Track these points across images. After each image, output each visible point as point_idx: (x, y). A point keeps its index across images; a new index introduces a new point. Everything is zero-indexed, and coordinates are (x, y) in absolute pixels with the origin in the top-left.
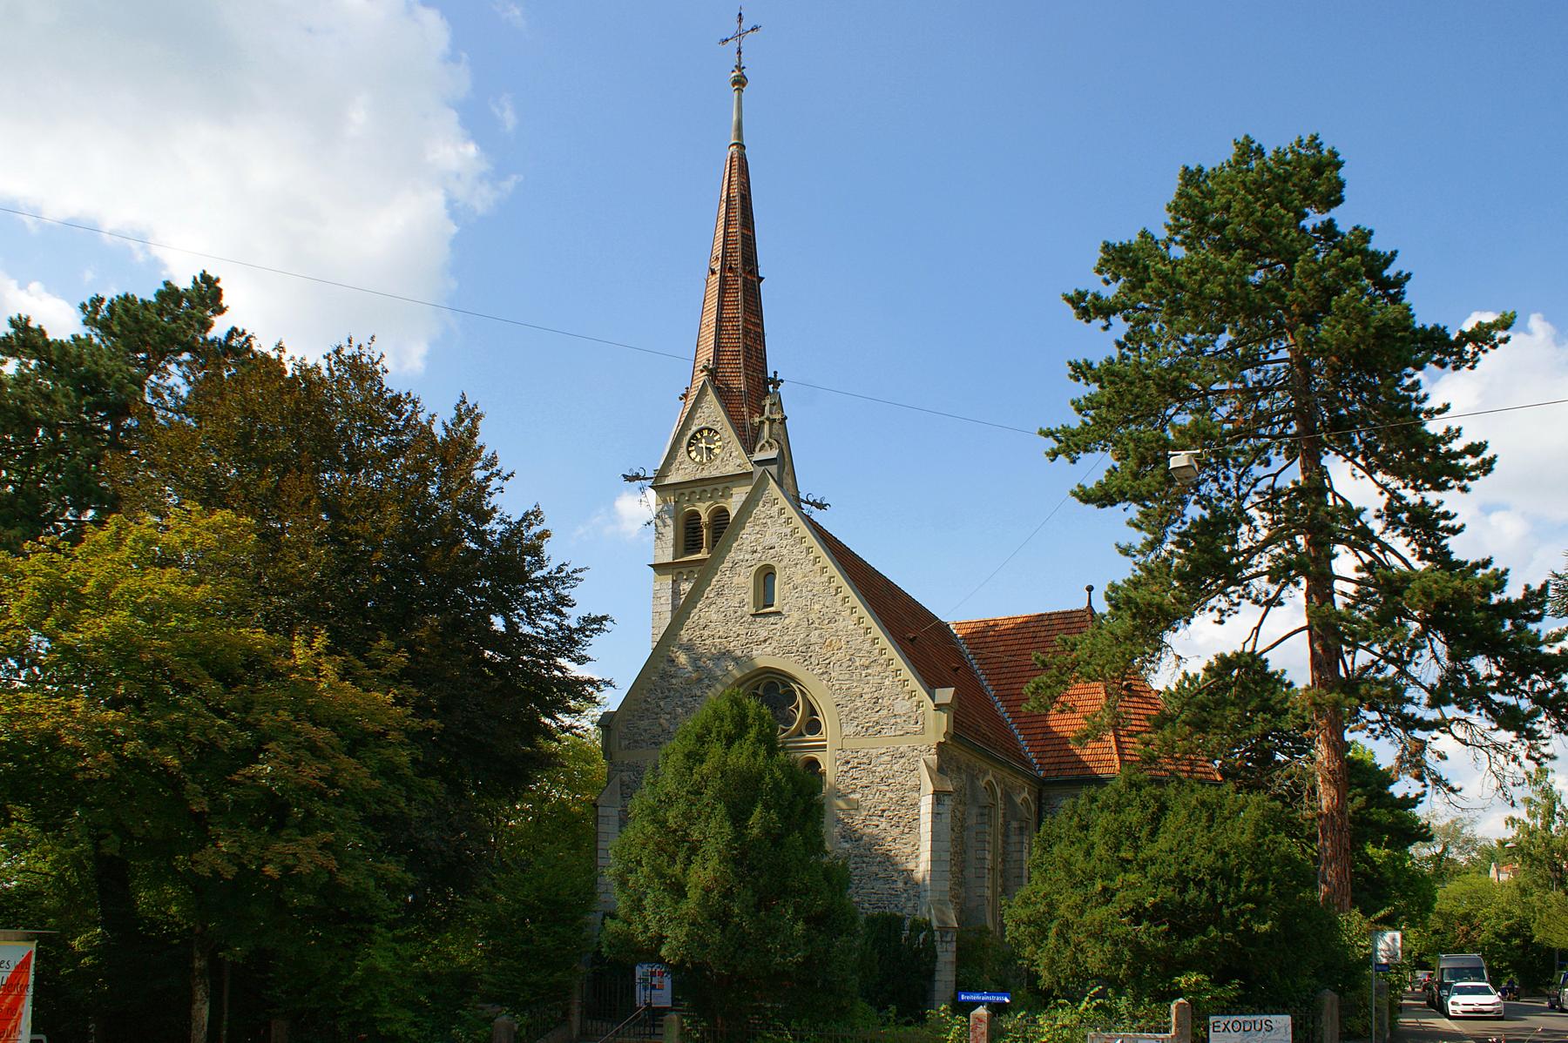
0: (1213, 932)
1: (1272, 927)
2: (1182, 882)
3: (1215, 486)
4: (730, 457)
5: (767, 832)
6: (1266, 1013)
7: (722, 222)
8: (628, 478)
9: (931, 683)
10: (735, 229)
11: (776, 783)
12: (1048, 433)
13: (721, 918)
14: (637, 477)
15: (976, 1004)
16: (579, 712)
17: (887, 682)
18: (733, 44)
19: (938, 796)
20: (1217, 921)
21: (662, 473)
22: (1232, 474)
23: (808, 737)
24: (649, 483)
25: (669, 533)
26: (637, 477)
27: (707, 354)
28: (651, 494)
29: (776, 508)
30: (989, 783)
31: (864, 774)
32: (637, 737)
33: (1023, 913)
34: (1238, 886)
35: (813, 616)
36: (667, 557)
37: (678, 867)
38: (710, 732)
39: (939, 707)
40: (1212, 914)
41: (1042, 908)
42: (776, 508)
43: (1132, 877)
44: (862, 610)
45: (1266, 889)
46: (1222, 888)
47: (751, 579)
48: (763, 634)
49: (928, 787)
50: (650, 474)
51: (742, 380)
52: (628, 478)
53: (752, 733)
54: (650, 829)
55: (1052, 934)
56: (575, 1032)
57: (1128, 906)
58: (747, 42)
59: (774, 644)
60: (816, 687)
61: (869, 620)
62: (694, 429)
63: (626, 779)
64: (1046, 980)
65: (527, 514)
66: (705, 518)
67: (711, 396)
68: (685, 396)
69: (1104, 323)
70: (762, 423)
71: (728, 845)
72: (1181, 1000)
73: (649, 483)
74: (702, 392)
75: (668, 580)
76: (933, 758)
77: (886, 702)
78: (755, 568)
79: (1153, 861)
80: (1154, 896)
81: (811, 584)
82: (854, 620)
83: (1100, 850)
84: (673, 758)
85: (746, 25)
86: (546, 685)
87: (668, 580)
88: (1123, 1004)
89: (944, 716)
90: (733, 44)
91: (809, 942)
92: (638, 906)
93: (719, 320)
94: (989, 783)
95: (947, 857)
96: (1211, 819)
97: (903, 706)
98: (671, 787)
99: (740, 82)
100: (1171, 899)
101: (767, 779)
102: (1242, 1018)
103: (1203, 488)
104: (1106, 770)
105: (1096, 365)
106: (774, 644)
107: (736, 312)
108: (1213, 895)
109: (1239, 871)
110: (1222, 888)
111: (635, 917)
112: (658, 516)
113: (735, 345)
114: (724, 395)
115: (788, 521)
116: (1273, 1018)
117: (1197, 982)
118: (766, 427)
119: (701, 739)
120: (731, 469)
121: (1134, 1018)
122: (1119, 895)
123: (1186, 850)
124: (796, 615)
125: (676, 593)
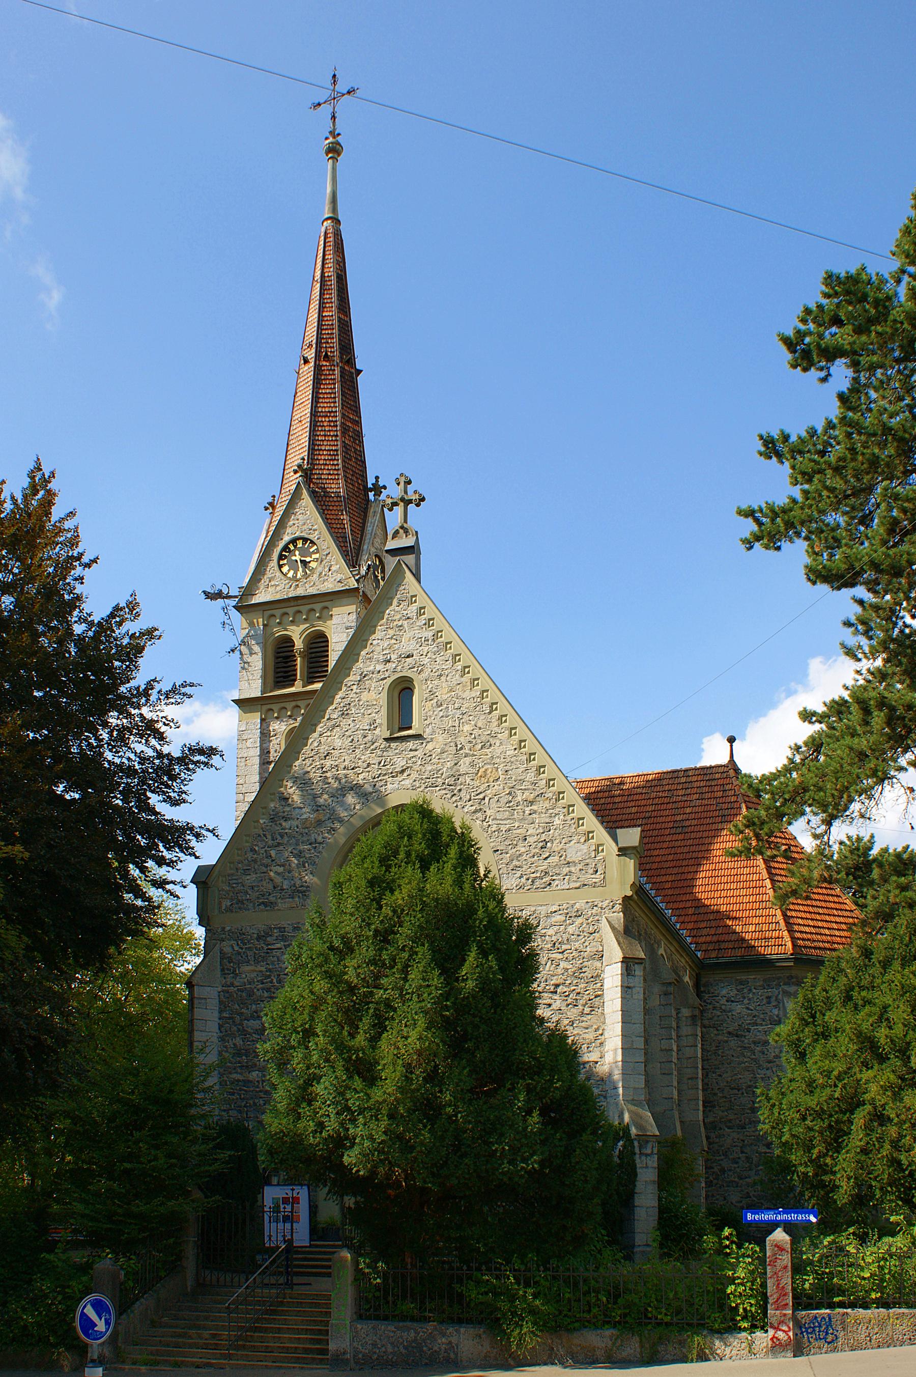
4: (330, 572)
5: (484, 984)
7: (315, 305)
8: (208, 595)
10: (332, 313)
12: (750, 513)
13: (428, 1109)
14: (219, 595)
15: (772, 1226)
16: (171, 864)
17: (557, 821)
18: (326, 109)
19: (628, 963)
21: (249, 590)
24: (233, 602)
25: (257, 662)
26: (219, 595)
27: (299, 453)
28: (235, 615)
29: (414, 607)
32: (241, 897)
35: (462, 740)
36: (254, 690)
37: (360, 1040)
38: (396, 853)
39: (623, 852)
42: (414, 607)
48: (400, 763)
49: (614, 952)
50: (234, 592)
51: (342, 486)
52: (209, 596)
54: (321, 985)
56: (190, 1283)
59: (414, 775)
62: (286, 538)
63: (227, 950)
65: (117, 608)
66: (299, 644)
67: (306, 500)
68: (272, 505)
73: (233, 602)
74: (295, 497)
75: (255, 719)
84: (349, 889)
85: (342, 87)
86: (133, 824)
87: (255, 719)
90: (326, 109)
92: (304, 1095)
93: (314, 414)
97: (577, 851)
98: (350, 926)
99: (334, 151)
104: (775, 950)
105: (793, 438)
106: (414, 775)
107: (333, 405)
111: (304, 1109)
112: (243, 643)
113: (331, 444)
114: (321, 499)
115: (429, 622)
119: (384, 861)
120: (330, 586)
124: (441, 739)
125: (265, 735)
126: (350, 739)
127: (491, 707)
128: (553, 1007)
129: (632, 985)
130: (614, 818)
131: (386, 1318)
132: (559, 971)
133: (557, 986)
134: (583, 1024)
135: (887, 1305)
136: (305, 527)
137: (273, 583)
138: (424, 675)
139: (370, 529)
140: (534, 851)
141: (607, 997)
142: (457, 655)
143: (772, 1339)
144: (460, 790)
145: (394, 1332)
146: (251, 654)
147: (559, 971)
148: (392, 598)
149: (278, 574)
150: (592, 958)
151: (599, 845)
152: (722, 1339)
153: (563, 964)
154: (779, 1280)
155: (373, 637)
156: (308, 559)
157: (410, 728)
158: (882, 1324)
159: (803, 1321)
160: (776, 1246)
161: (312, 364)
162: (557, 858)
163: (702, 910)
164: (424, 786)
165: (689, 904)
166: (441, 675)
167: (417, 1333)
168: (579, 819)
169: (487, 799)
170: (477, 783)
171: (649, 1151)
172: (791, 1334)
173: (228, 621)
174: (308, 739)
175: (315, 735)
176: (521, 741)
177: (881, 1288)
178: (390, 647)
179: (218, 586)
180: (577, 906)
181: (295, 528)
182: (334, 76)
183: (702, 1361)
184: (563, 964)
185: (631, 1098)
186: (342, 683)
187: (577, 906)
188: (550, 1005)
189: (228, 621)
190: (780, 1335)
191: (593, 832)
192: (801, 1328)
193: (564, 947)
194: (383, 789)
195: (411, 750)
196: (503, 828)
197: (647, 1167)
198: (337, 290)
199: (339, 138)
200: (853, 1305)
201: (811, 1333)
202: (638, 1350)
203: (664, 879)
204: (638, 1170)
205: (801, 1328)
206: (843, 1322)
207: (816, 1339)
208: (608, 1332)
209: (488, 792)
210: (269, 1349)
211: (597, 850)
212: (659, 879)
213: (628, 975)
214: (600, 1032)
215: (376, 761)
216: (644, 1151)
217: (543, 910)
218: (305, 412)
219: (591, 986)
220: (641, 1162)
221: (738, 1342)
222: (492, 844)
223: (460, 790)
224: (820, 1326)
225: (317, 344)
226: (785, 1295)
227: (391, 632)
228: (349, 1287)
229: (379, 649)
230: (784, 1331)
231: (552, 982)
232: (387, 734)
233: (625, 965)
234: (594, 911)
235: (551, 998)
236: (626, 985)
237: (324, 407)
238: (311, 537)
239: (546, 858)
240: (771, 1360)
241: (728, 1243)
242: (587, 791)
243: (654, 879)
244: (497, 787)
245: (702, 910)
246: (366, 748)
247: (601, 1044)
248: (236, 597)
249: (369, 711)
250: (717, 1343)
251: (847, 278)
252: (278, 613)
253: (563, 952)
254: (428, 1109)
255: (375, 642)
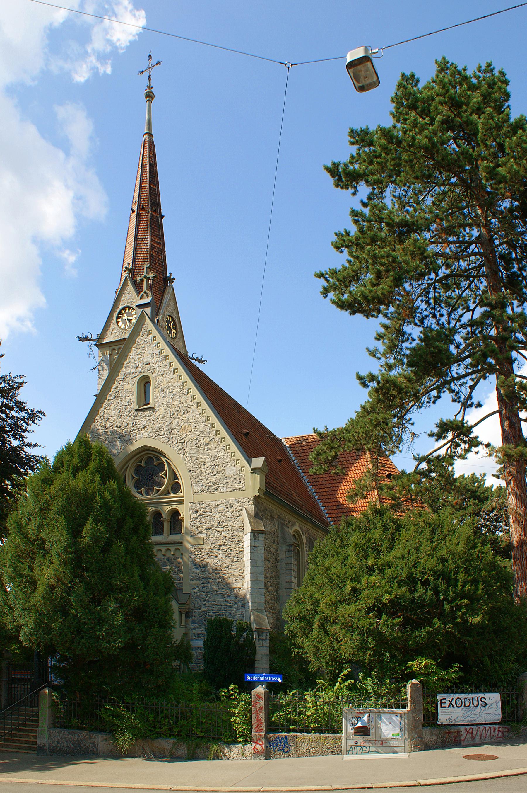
0: (437, 623)
1: (483, 619)
2: (411, 581)
3: (434, 321)
5: (96, 540)
6: (481, 692)
8: (80, 339)
9: (250, 454)
10: (146, 185)
11: (106, 503)
12: (321, 275)
13: (63, 609)
14: (86, 339)
18: (146, 74)
19: (254, 533)
20: (441, 615)
22: (445, 312)
23: (173, 495)
26: (86, 339)
27: (129, 259)
28: (96, 349)
29: (150, 337)
30: (296, 531)
31: (207, 519)
33: (295, 611)
34: (455, 586)
35: (173, 410)
39: (254, 471)
40: (436, 609)
41: (309, 606)
42: (150, 337)
43: (373, 579)
44: (204, 404)
45: (477, 589)
46: (443, 587)
47: (136, 386)
48: (143, 423)
49: (248, 528)
52: (80, 339)
53: (92, 465)
55: (315, 626)
57: (371, 602)
58: (145, 64)
60: (177, 460)
61: (209, 411)
62: (120, 307)
64: (313, 667)
69: (353, 190)
70: (142, 280)
71: (66, 549)
72: (414, 681)
73: (94, 342)
74: (125, 284)
76: (251, 507)
77: (220, 468)
78: (138, 378)
79: (389, 565)
80: (390, 594)
81: (172, 386)
82: (200, 410)
83: (352, 559)
85: (153, 62)
88: (369, 683)
89: (258, 477)
91: (130, 630)
93: (136, 240)
94: (296, 531)
95: (262, 578)
96: (433, 532)
97: (231, 470)
100: (403, 596)
101: (98, 497)
102: (462, 696)
103: (426, 321)
107: (146, 234)
108: (437, 593)
109: (456, 573)
110: (443, 587)
112: (100, 364)
113: (145, 256)
116: (487, 695)
117: (426, 666)
118: (145, 283)
121: (379, 696)
122: (365, 593)
123: (414, 556)
124: (163, 409)
126: (119, 411)
127: (188, 391)
128: (219, 557)
129: (257, 545)
130: (302, 458)
131: (66, 727)
132: (222, 537)
133: (220, 546)
134: (234, 567)
135: (321, 732)
136: (130, 301)
137: (114, 332)
138: (155, 374)
139: (165, 301)
140: (209, 471)
141: (245, 552)
142: (171, 363)
143: (254, 749)
144: (172, 438)
145: (68, 735)
146: (103, 370)
147: (222, 537)
148: (140, 332)
149: (117, 326)
150: (238, 530)
151: (242, 467)
152: (228, 747)
153: (223, 534)
154: (259, 715)
155: (130, 354)
156: (131, 318)
157: (149, 404)
158: (316, 742)
159: (271, 739)
160: (257, 695)
161: (136, 213)
162: (220, 474)
163: (341, 507)
164: (154, 436)
165: (334, 504)
166: (163, 374)
167: (79, 736)
168: (232, 453)
169: (186, 442)
170: (181, 433)
171: (264, 637)
172: (264, 746)
173: (92, 353)
174: (99, 411)
175: (102, 409)
176: (203, 410)
177: (317, 722)
178: (138, 359)
179: (86, 334)
180: (231, 501)
181: (124, 301)
182: (150, 55)
183: (218, 759)
184: (223, 534)
185: (256, 608)
186: (115, 380)
187: (231, 501)
188: (217, 556)
189: (92, 353)
190: (258, 746)
191: (239, 460)
192: (270, 743)
193: (224, 524)
194: (134, 438)
195: (148, 416)
196: (194, 458)
197: (263, 646)
198: (151, 173)
199: (152, 90)
200: (301, 731)
201: (275, 746)
202: (186, 751)
203: (323, 490)
204: (257, 648)
205: (270, 743)
206: (294, 741)
207: (278, 750)
208: (172, 740)
209: (186, 438)
210: (21, 742)
211: (241, 470)
212: (321, 490)
213: (255, 539)
214: (242, 571)
215: (131, 423)
216: (261, 637)
217: (213, 504)
218: (131, 239)
219: (238, 546)
220: (260, 643)
221: (236, 749)
222: (188, 467)
223: (172, 438)
224: (281, 742)
225: (138, 202)
226: (261, 724)
227: (139, 351)
228: (47, 709)
229: (133, 360)
230: (260, 745)
231: (218, 544)
232: (137, 408)
233: (252, 534)
234: (239, 504)
235: (217, 552)
236: (253, 545)
237: (141, 236)
238: (132, 306)
239: (215, 475)
240: (252, 761)
241: (232, 692)
242: (290, 443)
243: (318, 490)
244: (191, 436)
245: (341, 507)
246: (126, 416)
247: (243, 578)
248: (95, 340)
249: (128, 395)
250: (226, 749)
251: (361, 131)
252: (116, 348)
253: (223, 527)
254: (63, 609)
255: (131, 357)
